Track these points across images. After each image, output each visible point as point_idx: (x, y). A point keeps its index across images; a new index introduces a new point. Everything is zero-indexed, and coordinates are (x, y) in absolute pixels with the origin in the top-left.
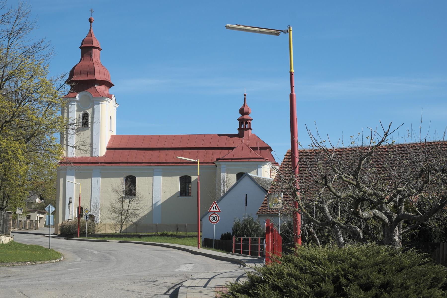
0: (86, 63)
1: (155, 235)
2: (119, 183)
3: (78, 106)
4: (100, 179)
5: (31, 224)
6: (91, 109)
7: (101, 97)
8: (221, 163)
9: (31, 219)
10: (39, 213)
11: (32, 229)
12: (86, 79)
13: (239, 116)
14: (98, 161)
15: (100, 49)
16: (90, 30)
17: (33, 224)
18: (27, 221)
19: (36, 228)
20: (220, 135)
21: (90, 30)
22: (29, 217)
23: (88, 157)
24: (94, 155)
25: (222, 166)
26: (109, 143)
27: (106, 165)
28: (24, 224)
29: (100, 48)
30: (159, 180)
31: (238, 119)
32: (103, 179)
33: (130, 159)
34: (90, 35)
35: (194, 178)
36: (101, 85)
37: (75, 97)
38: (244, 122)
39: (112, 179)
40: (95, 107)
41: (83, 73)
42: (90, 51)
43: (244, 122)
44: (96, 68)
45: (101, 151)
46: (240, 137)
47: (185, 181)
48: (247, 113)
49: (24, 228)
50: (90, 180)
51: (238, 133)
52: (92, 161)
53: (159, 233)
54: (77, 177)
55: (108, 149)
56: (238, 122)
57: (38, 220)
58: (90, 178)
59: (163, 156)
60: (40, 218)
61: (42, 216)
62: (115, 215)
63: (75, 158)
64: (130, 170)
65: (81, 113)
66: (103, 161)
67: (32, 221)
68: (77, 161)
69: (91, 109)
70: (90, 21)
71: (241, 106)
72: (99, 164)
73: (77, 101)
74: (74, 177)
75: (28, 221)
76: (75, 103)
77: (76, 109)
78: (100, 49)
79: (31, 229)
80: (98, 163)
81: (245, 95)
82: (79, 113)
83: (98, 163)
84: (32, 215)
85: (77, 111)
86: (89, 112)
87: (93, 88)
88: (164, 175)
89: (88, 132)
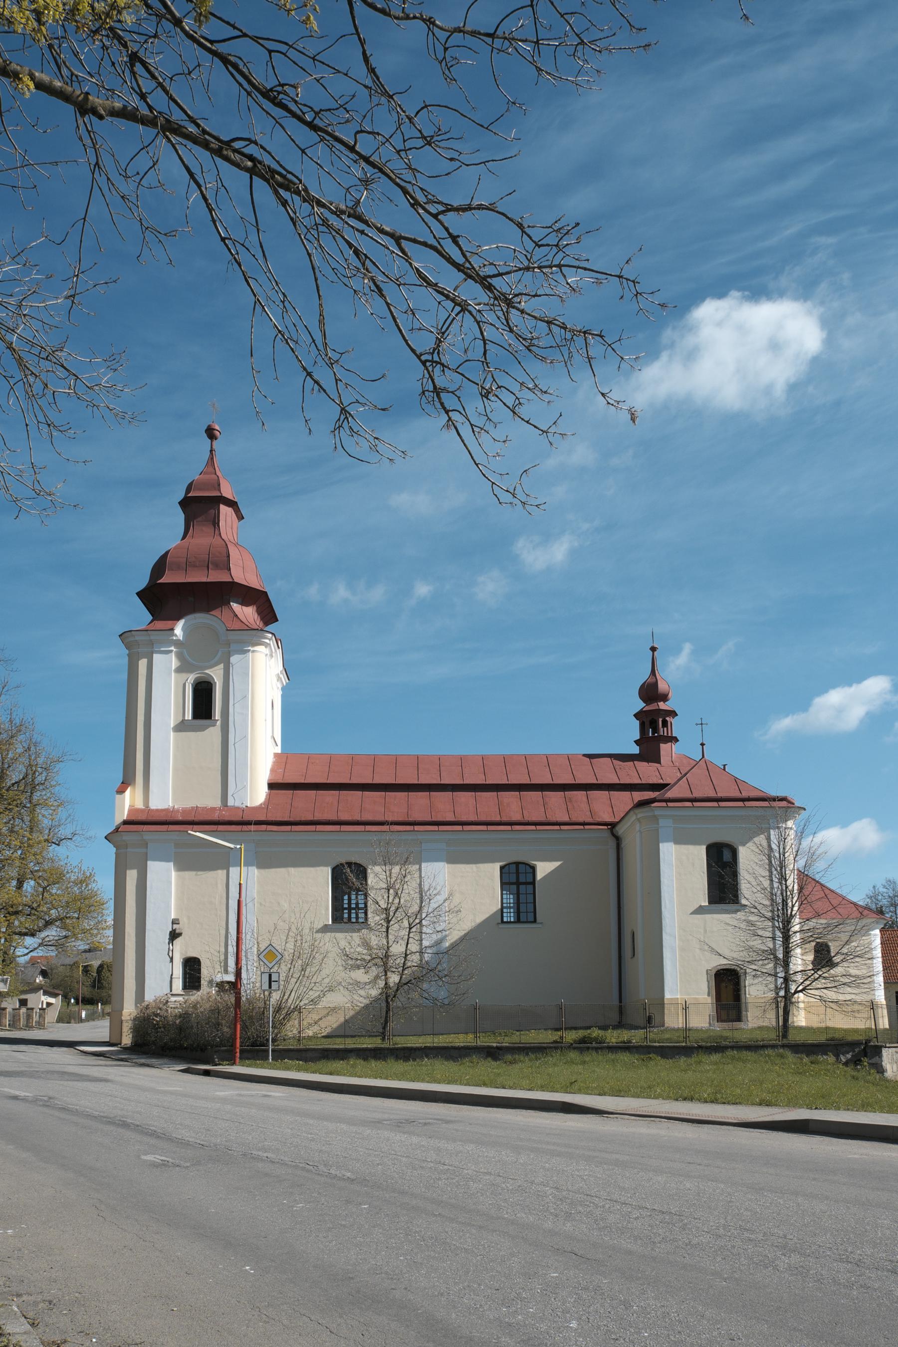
0: (202, 540)
1: (557, 1046)
2: (318, 883)
3: (179, 656)
4: (254, 871)
5: (29, 1017)
6: (222, 666)
7: (248, 637)
8: (658, 812)
9: (30, 1005)
10: (46, 993)
11: (32, 1027)
12: (204, 580)
13: (640, 705)
14: (246, 818)
15: (240, 517)
16: (211, 458)
17: (35, 1018)
18: (19, 1009)
19: (41, 1025)
20: (591, 756)
21: (211, 458)
22: (23, 1003)
23: (213, 809)
24: (231, 803)
25: (662, 822)
26: (273, 771)
27: (275, 828)
28: (14, 1016)
29: (244, 512)
30: (439, 875)
31: (636, 716)
32: (263, 871)
33: (339, 815)
34: (211, 469)
35: (543, 869)
36: (247, 606)
37: (172, 629)
38: (654, 724)
39: (292, 870)
40: (234, 659)
41: (195, 566)
42: (212, 511)
43: (654, 724)
44: (233, 552)
45: (255, 793)
46: (648, 760)
47: (517, 879)
48: (664, 698)
49: (14, 1025)
50: (221, 873)
51: (638, 752)
52: (227, 819)
53: (571, 1036)
54: (182, 866)
55: (272, 786)
56: (637, 723)
57: (45, 1006)
58: (222, 868)
59: (443, 806)
60: (49, 1004)
61: (52, 1000)
62: (360, 975)
63: (174, 811)
64: (350, 847)
65: (191, 678)
66: (263, 818)
67: (32, 1009)
68: (180, 818)
69: (222, 666)
70: (211, 433)
71: (644, 676)
72: (252, 827)
73: (177, 643)
74: (171, 864)
75: (23, 1010)
76: (172, 648)
77: (174, 663)
78: (240, 517)
79: (28, 1027)
80: (248, 823)
81: (653, 649)
82: (184, 676)
83: (248, 823)
84: (30, 997)
85: (179, 670)
86: (216, 674)
87: (225, 609)
88: (453, 859)
89: (213, 733)
